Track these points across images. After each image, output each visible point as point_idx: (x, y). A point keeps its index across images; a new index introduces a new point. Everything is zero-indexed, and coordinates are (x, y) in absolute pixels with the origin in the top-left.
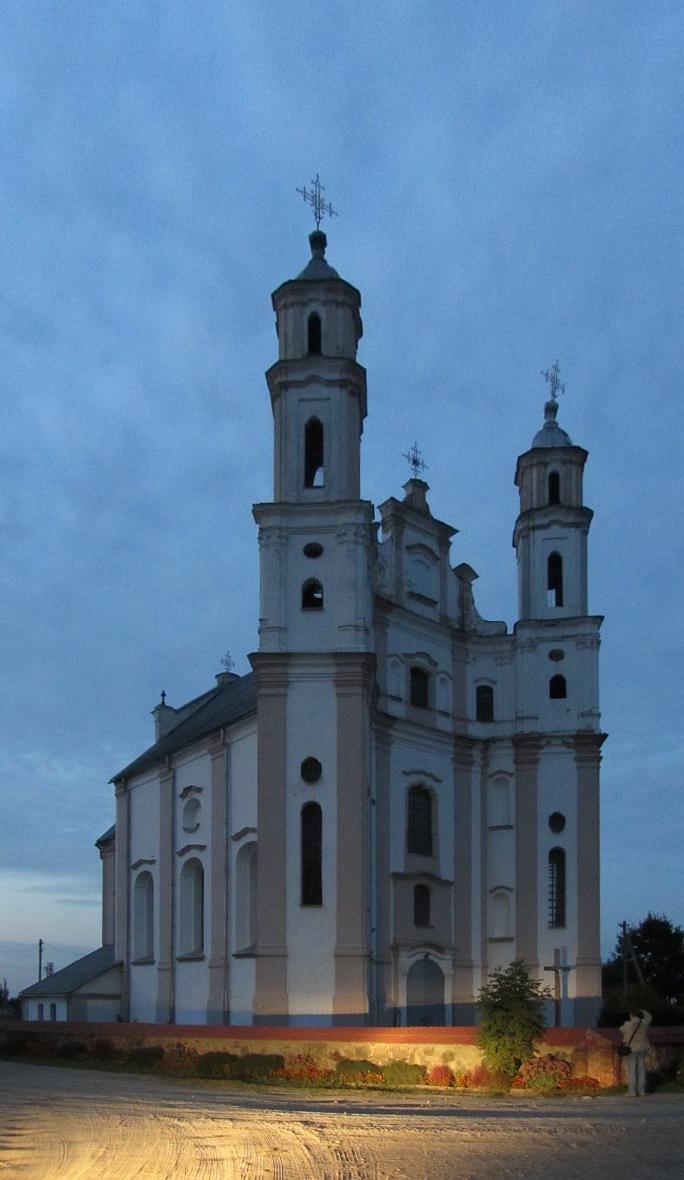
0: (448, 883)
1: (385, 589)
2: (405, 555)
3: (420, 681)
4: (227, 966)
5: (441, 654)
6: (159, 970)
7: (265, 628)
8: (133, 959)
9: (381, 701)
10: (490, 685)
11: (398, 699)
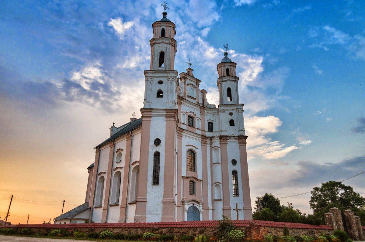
0: (200, 181)
1: (181, 95)
2: (186, 86)
3: (191, 120)
4: (126, 207)
5: (197, 112)
6: (103, 209)
7: (145, 102)
8: (95, 206)
10: (212, 122)
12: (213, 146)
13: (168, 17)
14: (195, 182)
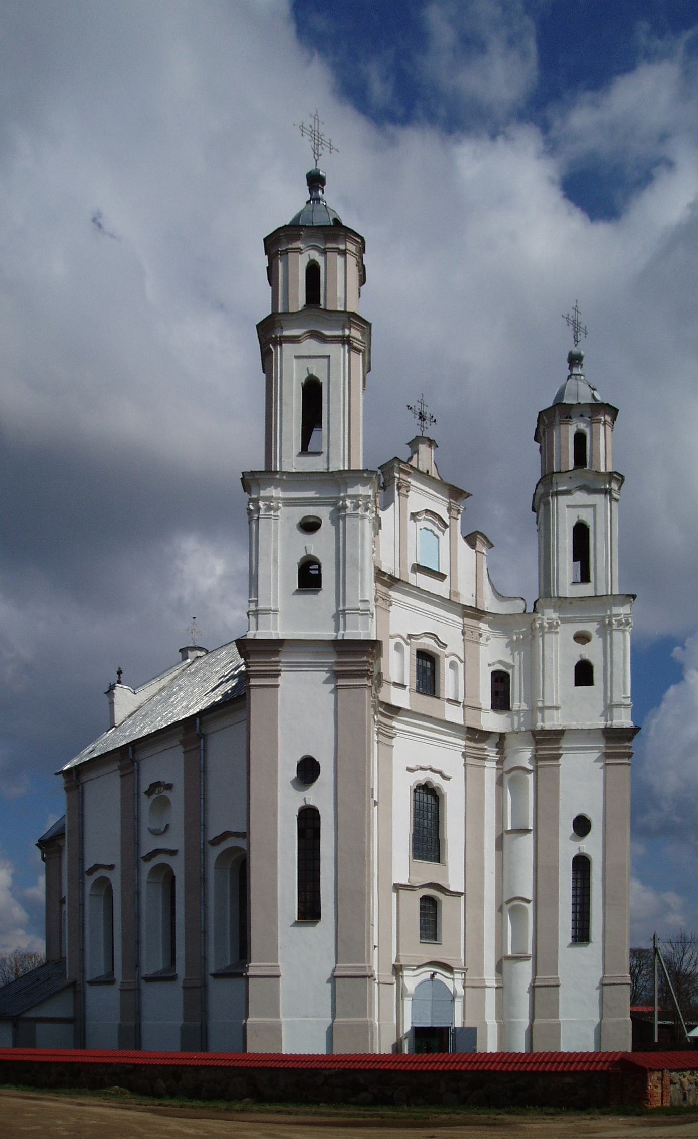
0: (459, 894)
9: (384, 688)
12: (507, 766)
13: (329, 195)
14: (441, 901)
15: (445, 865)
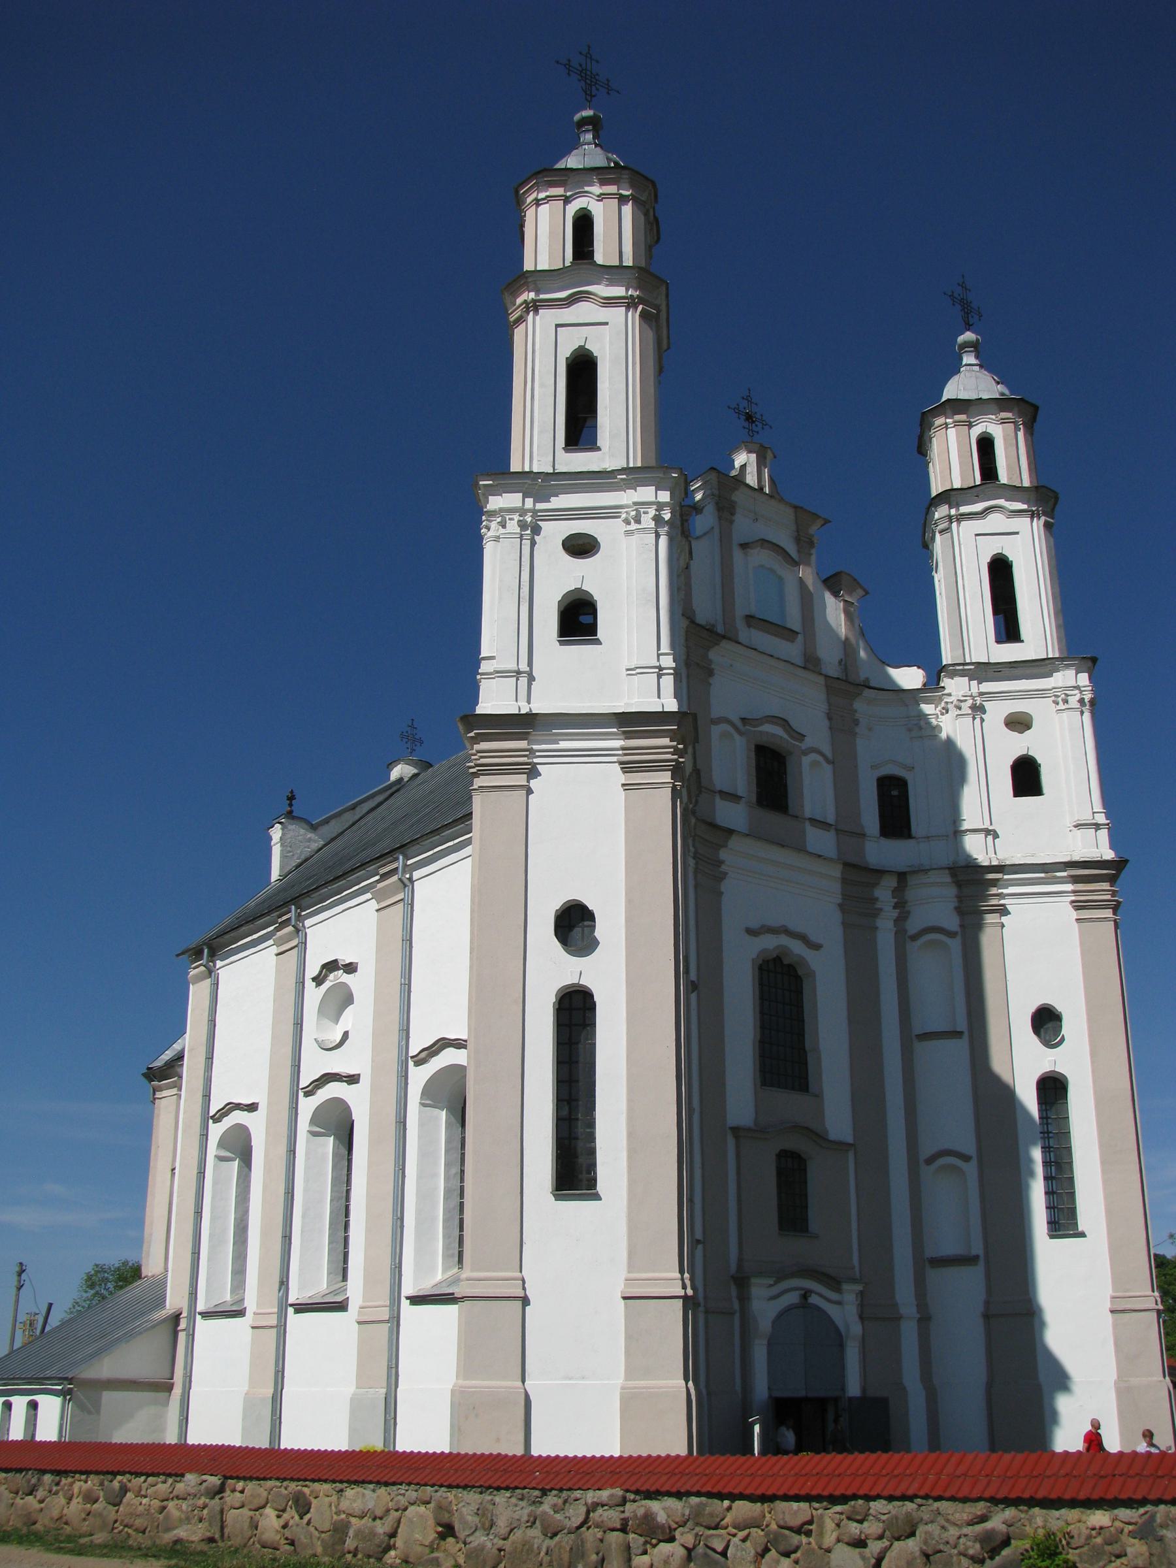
0: (842, 1146)
11: (734, 797)
12: (913, 926)
15: (819, 1096)
